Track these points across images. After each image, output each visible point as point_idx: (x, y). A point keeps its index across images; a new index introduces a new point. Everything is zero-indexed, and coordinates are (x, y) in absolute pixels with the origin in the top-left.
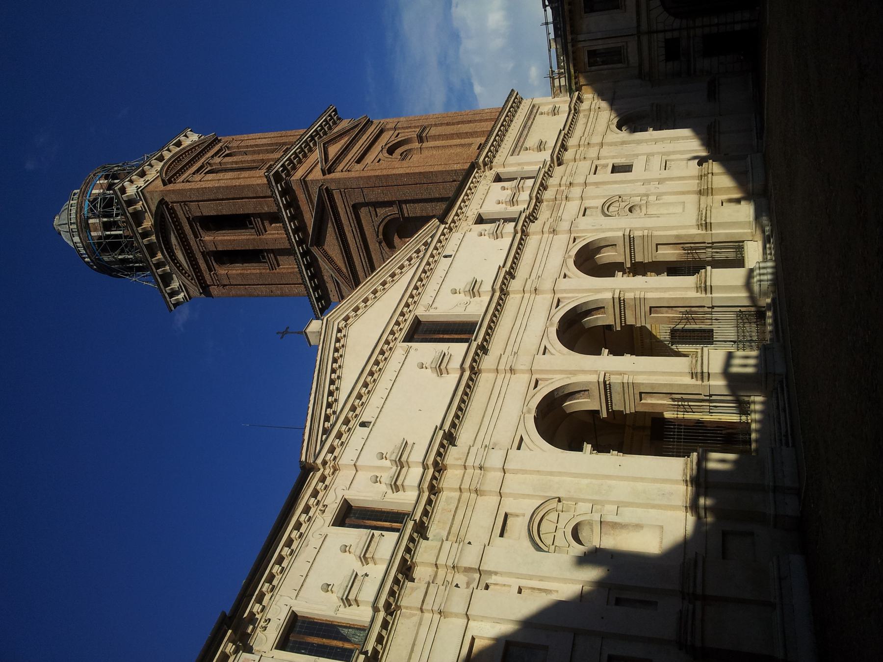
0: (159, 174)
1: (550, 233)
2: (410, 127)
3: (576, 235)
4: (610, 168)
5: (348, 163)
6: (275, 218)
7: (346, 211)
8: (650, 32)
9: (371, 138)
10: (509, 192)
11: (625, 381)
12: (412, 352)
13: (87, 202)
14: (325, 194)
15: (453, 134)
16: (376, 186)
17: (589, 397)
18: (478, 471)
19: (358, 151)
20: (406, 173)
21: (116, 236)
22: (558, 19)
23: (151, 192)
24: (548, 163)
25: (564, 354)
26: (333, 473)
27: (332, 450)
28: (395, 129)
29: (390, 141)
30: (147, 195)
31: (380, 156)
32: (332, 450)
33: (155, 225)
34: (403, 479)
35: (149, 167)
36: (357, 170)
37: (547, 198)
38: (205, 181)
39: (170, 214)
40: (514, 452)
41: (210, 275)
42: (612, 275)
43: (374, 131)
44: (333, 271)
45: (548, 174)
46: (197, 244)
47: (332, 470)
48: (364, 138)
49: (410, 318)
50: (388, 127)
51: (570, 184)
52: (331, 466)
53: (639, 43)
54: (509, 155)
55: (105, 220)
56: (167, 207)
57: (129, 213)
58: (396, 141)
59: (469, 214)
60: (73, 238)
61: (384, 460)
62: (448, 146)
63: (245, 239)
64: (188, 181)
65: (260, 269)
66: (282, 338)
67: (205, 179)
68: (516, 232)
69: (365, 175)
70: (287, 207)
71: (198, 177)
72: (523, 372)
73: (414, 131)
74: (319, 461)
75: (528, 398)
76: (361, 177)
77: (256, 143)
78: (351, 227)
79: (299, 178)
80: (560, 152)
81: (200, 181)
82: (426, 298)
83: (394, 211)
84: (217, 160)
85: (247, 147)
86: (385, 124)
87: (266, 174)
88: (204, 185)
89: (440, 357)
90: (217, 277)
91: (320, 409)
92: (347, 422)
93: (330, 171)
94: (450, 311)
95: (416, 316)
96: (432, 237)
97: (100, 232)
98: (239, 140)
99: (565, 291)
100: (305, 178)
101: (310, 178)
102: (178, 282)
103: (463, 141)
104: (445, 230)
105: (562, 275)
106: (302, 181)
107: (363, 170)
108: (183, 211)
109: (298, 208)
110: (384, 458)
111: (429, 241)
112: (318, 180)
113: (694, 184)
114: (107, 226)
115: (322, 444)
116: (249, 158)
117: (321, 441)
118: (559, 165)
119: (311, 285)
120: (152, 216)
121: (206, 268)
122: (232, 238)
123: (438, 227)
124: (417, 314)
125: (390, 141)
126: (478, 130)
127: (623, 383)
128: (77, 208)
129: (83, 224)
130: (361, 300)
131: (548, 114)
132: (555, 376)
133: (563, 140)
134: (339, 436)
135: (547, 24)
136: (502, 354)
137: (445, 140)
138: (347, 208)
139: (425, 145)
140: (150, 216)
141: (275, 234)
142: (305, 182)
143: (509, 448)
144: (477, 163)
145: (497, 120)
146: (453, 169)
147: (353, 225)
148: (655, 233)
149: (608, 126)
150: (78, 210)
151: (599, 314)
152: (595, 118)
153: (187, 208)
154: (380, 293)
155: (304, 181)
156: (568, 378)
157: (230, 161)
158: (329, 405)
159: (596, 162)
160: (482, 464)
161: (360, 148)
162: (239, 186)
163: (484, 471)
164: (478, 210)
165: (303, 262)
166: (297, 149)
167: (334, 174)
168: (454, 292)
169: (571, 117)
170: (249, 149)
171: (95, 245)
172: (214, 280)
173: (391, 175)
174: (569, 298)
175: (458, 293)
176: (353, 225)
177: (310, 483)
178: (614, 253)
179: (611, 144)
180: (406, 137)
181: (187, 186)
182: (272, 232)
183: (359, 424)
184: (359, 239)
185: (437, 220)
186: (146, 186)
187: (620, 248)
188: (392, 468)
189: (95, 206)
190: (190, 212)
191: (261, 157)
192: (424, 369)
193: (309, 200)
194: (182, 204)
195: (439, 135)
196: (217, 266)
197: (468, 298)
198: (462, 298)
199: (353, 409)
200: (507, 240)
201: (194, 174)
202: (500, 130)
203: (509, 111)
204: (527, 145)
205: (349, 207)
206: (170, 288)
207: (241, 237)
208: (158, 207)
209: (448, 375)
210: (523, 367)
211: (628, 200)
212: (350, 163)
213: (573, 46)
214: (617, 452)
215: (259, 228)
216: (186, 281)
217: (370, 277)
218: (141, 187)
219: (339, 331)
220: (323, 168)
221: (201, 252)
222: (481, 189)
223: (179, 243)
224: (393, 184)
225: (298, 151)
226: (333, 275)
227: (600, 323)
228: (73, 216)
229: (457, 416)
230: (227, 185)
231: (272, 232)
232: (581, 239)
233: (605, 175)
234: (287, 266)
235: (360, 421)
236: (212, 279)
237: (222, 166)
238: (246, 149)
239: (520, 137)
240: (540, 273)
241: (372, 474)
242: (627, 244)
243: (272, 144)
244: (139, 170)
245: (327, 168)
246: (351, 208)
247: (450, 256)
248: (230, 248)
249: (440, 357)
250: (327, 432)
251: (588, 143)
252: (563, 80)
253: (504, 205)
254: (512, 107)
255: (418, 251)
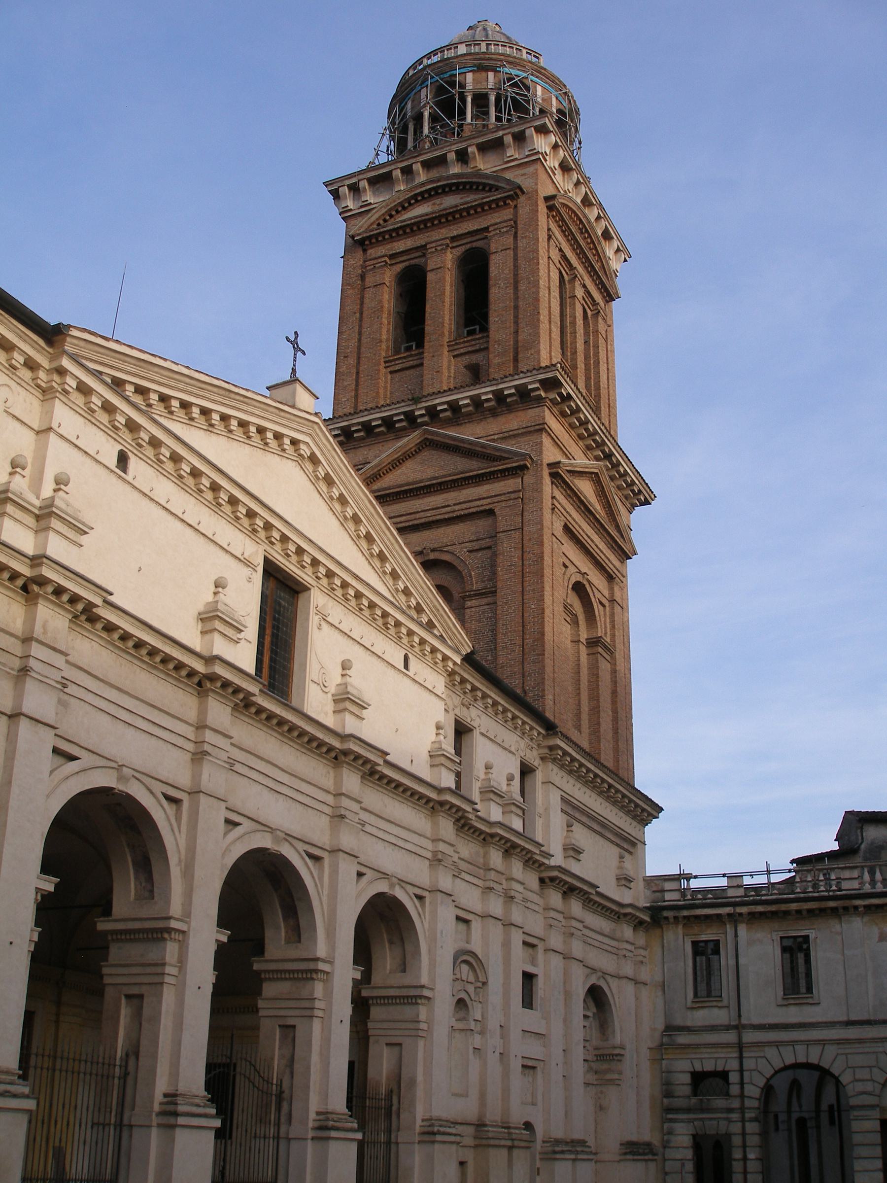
0: (562, 192)
1: (435, 853)
2: (613, 627)
3: (427, 900)
4: (530, 969)
5: (565, 510)
6: (476, 374)
7: (484, 498)
8: (740, 1047)
9: (601, 557)
10: (504, 788)
11: (168, 970)
12: (247, 571)
13: (525, 75)
14: (517, 464)
15: (598, 700)
16: (525, 555)
17: (138, 898)
18: (17, 664)
19: (583, 530)
20: (543, 609)
21: (462, 113)
22: (775, 891)
23: (535, 174)
24: (546, 861)
25: (223, 855)
26: (39, 386)
27: (83, 389)
28: (612, 601)
29: (594, 589)
30: (530, 169)
31: (572, 569)
32: (83, 389)
33: (478, 173)
34: (15, 516)
35: (575, 180)
36: (553, 525)
37: (492, 854)
38: (549, 265)
39: (496, 201)
40: (49, 740)
41: (383, 256)
42: (356, 962)
43: (611, 563)
44: (376, 466)
45: (530, 862)
46: (439, 240)
47: (43, 385)
48: (602, 545)
49: (305, 576)
50: (616, 589)
51: (512, 897)
52: (54, 384)
53: (727, 1028)
54: (564, 794)
55: (492, 98)
56: (509, 197)
57: (503, 135)
58: (593, 600)
59: (474, 712)
60: (464, 45)
61: (54, 486)
62: (579, 689)
63: (443, 319)
64: (549, 237)
65: (387, 340)
66: (287, 338)
67: (552, 265)
68: (440, 790)
69: (545, 536)
70: (499, 397)
71: (555, 255)
72: (196, 777)
73: (606, 633)
74: (66, 363)
75: (147, 780)
76: (542, 529)
77: (601, 363)
78: (455, 505)
79: (546, 421)
80: (562, 884)
81: (549, 257)
82: (337, 612)
83: (476, 583)
84: (579, 293)
85: (597, 347)
86: (621, 585)
87: (559, 365)
88: (543, 262)
89: (236, 621)
90: (379, 267)
91: (161, 380)
92: (132, 426)
93: (555, 476)
94: (313, 653)
95: (310, 589)
96: (441, 638)
97: (471, 88)
98: (606, 336)
99: (335, 872)
100: (546, 431)
101: (546, 441)
102: (376, 201)
103: (585, 717)
104: (450, 664)
105: (363, 870)
106: (541, 427)
107: (553, 534)
108: (500, 223)
109: (494, 413)
110: (58, 487)
111: (436, 632)
112: (541, 453)
113: (493, 1114)
114: (480, 100)
115: (96, 373)
116: (580, 346)
117: (101, 373)
118: (542, 881)
119: (353, 425)
120: (494, 172)
121: (398, 251)
122: (447, 300)
123: (457, 651)
124: (312, 590)
125: (594, 589)
126: (602, 745)
127: (164, 964)
128: (515, 57)
129: (486, 63)
130: (344, 493)
131: (620, 868)
132: (184, 836)
133: (581, 890)
134: (108, 408)
135: (768, 872)
136: (232, 741)
137: (589, 685)
138: (488, 501)
139: (583, 650)
140: (495, 169)
141: (449, 372)
142: (541, 430)
143: (57, 732)
144: (555, 734)
145: (614, 774)
146: (546, 692)
147: (457, 508)
148: (317, 1025)
149: (594, 970)
150: (511, 59)
151: (286, 932)
152: (609, 949)
153: (505, 229)
154: (353, 530)
155: (541, 428)
156: (180, 861)
157: (577, 314)
158: (164, 399)
159: (541, 946)
160: (33, 674)
161: (587, 535)
162: (538, 320)
163: (18, 676)
164: (478, 729)
165: (396, 411)
166: (593, 426)
167: (550, 483)
168: (346, 666)
169: (614, 907)
170: (592, 348)
171: (451, 76)
172: (375, 262)
173: (543, 583)
174: (321, 878)
175: (344, 672)
176: (457, 508)
177: (26, 338)
178: (388, 967)
179: (566, 973)
180: (598, 618)
181: (543, 235)
182: (453, 367)
183: (125, 449)
184: (431, 516)
185: (469, 651)
186: (546, 169)
187: (399, 979)
188: (38, 498)
189: (515, 85)
190: (497, 234)
191: (581, 366)
192: (212, 588)
193: (506, 435)
194: (512, 223)
195: (597, 676)
196: (399, 270)
197: (332, 689)
198: (335, 678)
199: (155, 443)
200: (425, 773)
201: (560, 250)
202: (603, 780)
203: (631, 801)
204: (577, 827)
205: (490, 504)
206: (367, 187)
207: (447, 312)
208: (508, 182)
209: (199, 632)
210: (205, 777)
211: (477, 999)
212: (565, 514)
213: (729, 915)
214: (37, 940)
215: (462, 346)
216: (377, 216)
217: (382, 514)
218: (546, 160)
219: (294, 442)
220: (561, 465)
221: (425, 245)
222: (511, 739)
223: (445, 209)
224: (526, 584)
225: (590, 427)
226: (369, 466)
227: (269, 934)
228: (501, 50)
229: (125, 637)
230: (541, 300)
231: (453, 367)
232: (420, 910)
233: (520, 962)
234: (389, 388)
235: (130, 454)
236: (376, 258)
237: (568, 300)
238: (591, 345)
239: (589, 816)
240: (368, 828)
241: (30, 461)
242: (404, 992)
243: (598, 388)
244: (572, 163)
245: (560, 472)
246: (487, 507)
247: (406, 666)
248: (430, 294)
249: (236, 621)
250: (117, 384)
251: (573, 934)
252: (676, 896)
253: (482, 776)
254: (637, 805)
255: (419, 609)
